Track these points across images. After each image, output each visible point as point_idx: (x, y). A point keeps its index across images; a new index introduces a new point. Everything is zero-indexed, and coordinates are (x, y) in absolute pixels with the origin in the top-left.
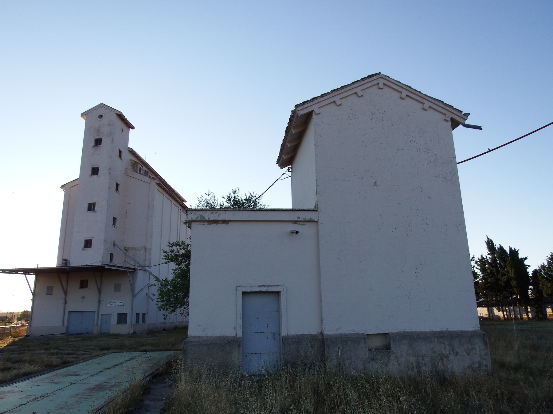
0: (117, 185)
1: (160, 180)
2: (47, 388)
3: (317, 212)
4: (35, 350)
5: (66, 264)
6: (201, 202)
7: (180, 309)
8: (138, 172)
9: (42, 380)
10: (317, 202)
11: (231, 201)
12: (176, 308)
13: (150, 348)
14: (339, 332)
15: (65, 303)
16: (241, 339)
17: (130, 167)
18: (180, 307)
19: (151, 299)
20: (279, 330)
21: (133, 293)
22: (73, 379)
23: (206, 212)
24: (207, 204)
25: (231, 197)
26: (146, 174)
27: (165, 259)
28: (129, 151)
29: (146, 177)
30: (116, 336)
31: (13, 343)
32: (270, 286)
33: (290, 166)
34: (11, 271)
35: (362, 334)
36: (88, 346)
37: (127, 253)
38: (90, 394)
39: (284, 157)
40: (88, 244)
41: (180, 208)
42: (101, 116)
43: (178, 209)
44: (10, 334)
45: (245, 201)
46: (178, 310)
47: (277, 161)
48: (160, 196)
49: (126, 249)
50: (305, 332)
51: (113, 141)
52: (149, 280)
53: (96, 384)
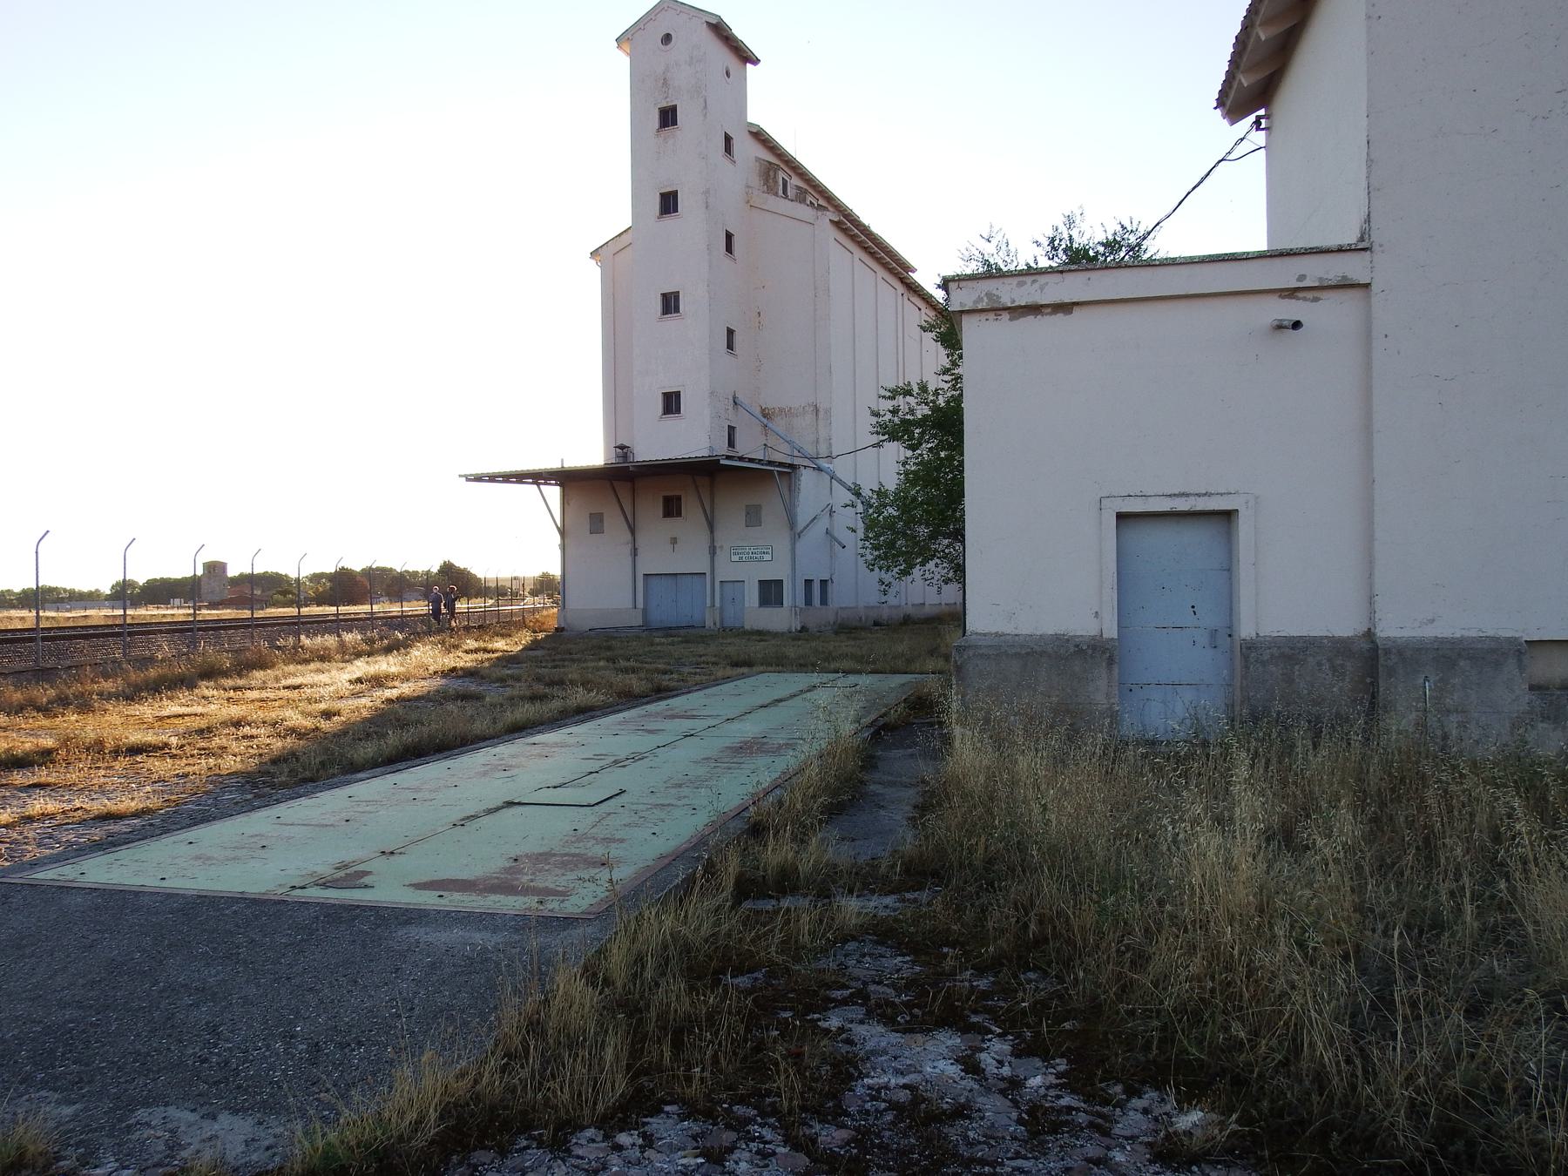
0: (729, 237)
1: (840, 211)
2: (643, 743)
3: (1368, 252)
4: (585, 661)
5: (625, 456)
6: (968, 263)
7: (923, 568)
8: (780, 192)
9: (620, 723)
10: (1368, 220)
11: (1060, 253)
12: (912, 566)
13: (846, 664)
14: (1430, 632)
15: (635, 552)
16: (1117, 644)
17: (756, 181)
18: (923, 564)
19: (840, 543)
20: (1231, 620)
21: (792, 529)
22: (687, 725)
23: (1003, 283)
24: (986, 267)
25: (1061, 240)
26: (801, 197)
27: (878, 433)
28: (751, 132)
29: (802, 205)
30: (761, 635)
31: (535, 645)
32: (1205, 494)
33: (1263, 110)
34: (507, 478)
35: (1512, 641)
36: (701, 656)
37: (770, 425)
38: (735, 760)
39: (1245, 80)
40: (671, 403)
41: (901, 288)
42: (667, 39)
43: (896, 294)
44: (523, 625)
45: (1101, 249)
46: (917, 572)
47: (1217, 97)
48: (844, 260)
49: (766, 414)
50: (1317, 630)
51: (705, 107)
52: (831, 494)
53: (743, 739)
